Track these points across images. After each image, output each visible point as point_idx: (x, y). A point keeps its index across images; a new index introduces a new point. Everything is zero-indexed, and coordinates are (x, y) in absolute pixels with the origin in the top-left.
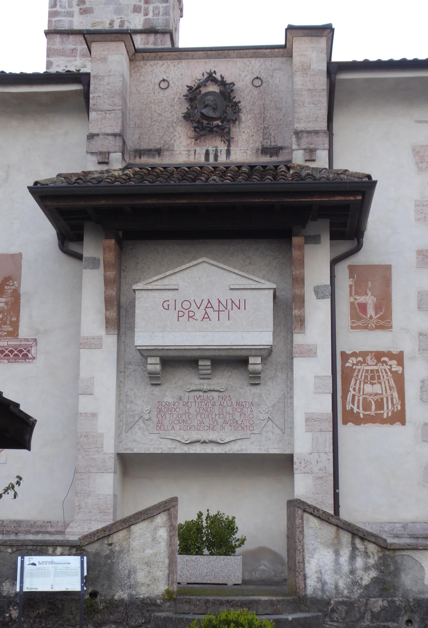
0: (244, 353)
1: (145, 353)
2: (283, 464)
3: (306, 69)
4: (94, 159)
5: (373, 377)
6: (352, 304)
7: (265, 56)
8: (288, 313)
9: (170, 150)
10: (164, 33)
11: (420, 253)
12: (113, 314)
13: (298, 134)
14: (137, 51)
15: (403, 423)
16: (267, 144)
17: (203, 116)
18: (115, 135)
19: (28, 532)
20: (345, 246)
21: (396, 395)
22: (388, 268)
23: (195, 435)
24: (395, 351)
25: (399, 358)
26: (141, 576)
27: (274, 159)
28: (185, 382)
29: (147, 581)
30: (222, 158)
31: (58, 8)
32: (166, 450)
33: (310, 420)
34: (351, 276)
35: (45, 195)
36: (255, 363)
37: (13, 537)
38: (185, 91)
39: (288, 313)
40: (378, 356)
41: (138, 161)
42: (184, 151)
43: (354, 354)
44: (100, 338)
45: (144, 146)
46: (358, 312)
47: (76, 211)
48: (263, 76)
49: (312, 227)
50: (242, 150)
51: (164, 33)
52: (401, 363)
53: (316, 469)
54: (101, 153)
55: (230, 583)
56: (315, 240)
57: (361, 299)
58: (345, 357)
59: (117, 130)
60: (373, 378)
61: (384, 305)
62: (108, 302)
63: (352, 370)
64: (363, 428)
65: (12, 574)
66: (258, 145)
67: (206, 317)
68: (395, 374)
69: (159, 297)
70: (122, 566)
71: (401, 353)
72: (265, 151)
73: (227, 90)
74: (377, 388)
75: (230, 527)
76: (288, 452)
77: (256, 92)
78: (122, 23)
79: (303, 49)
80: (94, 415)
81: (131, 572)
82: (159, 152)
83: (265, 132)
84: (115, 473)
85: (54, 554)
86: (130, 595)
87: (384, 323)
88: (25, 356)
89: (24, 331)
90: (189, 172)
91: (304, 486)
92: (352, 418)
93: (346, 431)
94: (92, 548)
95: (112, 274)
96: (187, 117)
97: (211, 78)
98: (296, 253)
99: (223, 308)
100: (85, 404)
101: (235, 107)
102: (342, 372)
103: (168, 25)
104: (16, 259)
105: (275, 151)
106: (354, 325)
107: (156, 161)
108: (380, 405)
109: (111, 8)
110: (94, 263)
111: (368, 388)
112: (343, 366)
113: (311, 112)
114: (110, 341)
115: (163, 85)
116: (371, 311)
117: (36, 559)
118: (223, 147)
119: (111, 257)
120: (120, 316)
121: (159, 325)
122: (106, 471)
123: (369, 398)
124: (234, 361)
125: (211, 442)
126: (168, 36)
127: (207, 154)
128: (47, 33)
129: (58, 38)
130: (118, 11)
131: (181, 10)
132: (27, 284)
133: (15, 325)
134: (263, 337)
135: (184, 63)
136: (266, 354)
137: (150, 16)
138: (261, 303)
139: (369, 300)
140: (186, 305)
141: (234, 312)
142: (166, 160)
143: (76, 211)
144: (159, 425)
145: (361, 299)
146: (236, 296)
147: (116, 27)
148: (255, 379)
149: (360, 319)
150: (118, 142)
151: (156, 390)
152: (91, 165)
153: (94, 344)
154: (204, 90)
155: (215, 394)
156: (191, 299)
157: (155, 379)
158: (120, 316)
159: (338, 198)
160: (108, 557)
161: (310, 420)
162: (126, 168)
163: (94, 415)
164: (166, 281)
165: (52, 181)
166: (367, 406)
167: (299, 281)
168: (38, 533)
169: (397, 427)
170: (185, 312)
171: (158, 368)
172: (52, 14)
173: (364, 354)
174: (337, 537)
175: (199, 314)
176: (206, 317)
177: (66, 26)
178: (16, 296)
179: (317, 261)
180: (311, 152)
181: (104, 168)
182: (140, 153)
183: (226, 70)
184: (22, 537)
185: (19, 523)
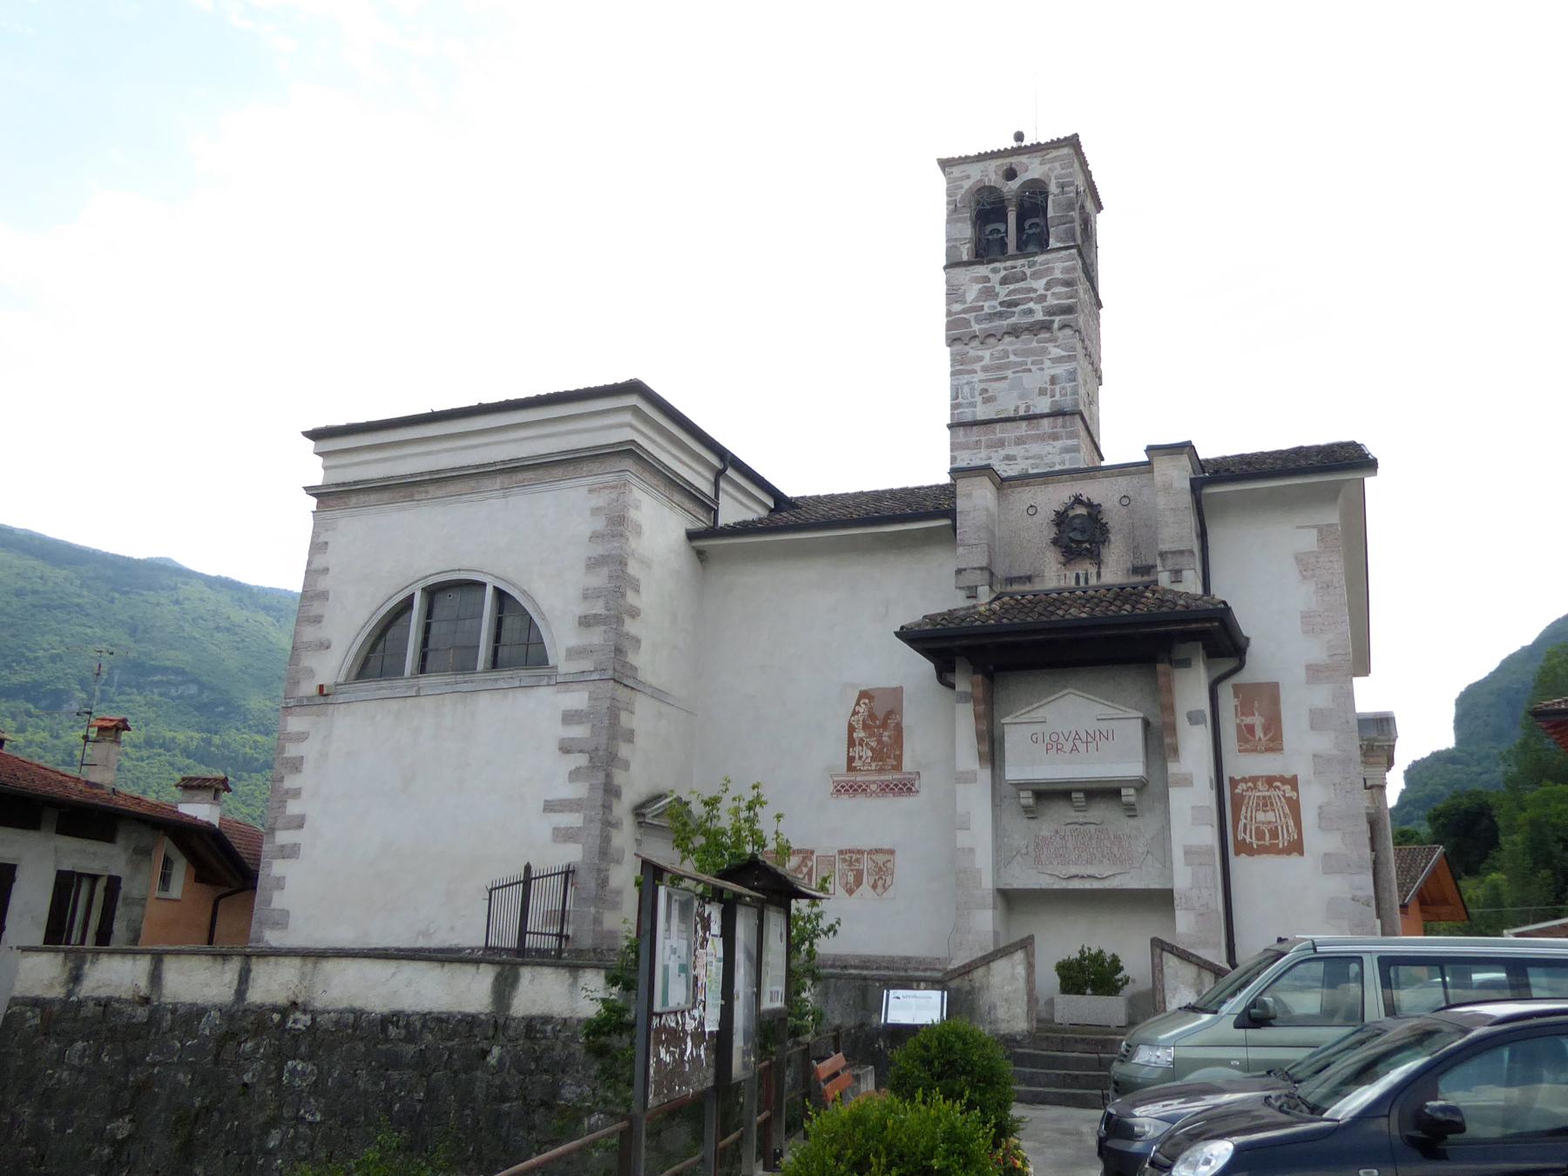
0: (1115, 785)
1: (1020, 786)
2: (1162, 900)
3: (1167, 488)
4: (963, 594)
5: (1265, 804)
6: (1239, 726)
7: (1130, 474)
8: (1159, 740)
9: (1041, 576)
10: (1072, 414)
11: (1309, 667)
12: (986, 748)
13: (1162, 555)
14: (1003, 480)
15: (1302, 854)
16: (1138, 563)
17: (1072, 540)
18: (982, 569)
19: (917, 969)
20: (1227, 664)
21: (1291, 823)
22: (1276, 685)
23: (1073, 870)
24: (1288, 775)
25: (1293, 782)
26: (1001, 1013)
27: (1146, 578)
28: (1059, 816)
29: (1006, 1017)
30: (1093, 581)
31: (960, 400)
32: (1044, 886)
33: (1189, 852)
34: (1236, 696)
35: (912, 637)
36: (1128, 794)
37: (902, 973)
38: (1053, 516)
39: (1159, 740)
40: (1270, 781)
41: (1009, 589)
42: (1054, 575)
43: (1244, 780)
44: (974, 773)
45: (1015, 574)
46: (1246, 733)
47: (944, 645)
48: (1131, 494)
49: (1181, 651)
50: (1113, 571)
51: (1072, 414)
52: (1295, 788)
53: (1197, 906)
54: (969, 588)
55: (1113, 1025)
56: (1186, 663)
57: (1248, 720)
58: (1234, 783)
59: (984, 564)
60: (1265, 805)
61: (1274, 725)
62: (980, 736)
63: (1242, 797)
64: (1257, 859)
65: (878, 1007)
66: (1129, 565)
67: (1075, 749)
68: (1289, 800)
69: (1027, 731)
70: (984, 1001)
71: (1295, 778)
72: (1136, 570)
73: (1094, 510)
74: (1270, 816)
75: (1116, 965)
76: (1168, 886)
77: (1124, 510)
78: (1028, 407)
79: (1163, 466)
80: (972, 850)
81: (992, 1008)
82: (1029, 579)
83: (1136, 551)
84: (995, 908)
85: (918, 988)
86: (991, 1031)
87: (1274, 743)
88: (910, 790)
89: (907, 765)
90: (1059, 598)
91: (1185, 926)
92: (1244, 848)
93: (1238, 863)
94: (954, 984)
95: (981, 708)
96: (1055, 542)
97: (1078, 500)
98: (1162, 680)
99: (1092, 738)
100: (963, 840)
101: (1104, 529)
102: (1227, 797)
103: (1077, 404)
104: (897, 692)
105: (1147, 570)
106: (887, 857)
107: (1027, 587)
108: (1274, 834)
109: (1015, 393)
110: (964, 698)
111: (1261, 816)
112: (1233, 794)
113: (1177, 530)
114: (985, 775)
115: (1031, 511)
116: (1259, 733)
117: (900, 993)
118: (1093, 570)
119: (979, 692)
120: (992, 750)
121: (1028, 762)
122: (984, 907)
123: (1263, 827)
124: (1105, 793)
125: (1090, 876)
126: (1078, 418)
127: (1078, 576)
128: (950, 427)
129: (961, 431)
130: (1022, 396)
131: (1100, 378)
132: (909, 719)
133: (899, 759)
134: (1131, 767)
135: (1051, 487)
136: (1141, 786)
137: (1057, 397)
138: (1132, 732)
139: (1257, 721)
140: (1054, 737)
141: (1103, 744)
142: (1037, 586)
143: (944, 645)
144: (1037, 860)
145: (1248, 720)
146: (1104, 726)
147: (1022, 413)
148: (1131, 810)
149: (1247, 741)
150: (986, 575)
151: (1033, 823)
152: (959, 601)
153: (967, 778)
154: (1071, 513)
155: (1092, 827)
156: (1059, 731)
157: (1030, 813)
158: (992, 750)
159: (1194, 626)
160: (969, 993)
161: (1189, 852)
162: (997, 598)
163: (972, 850)
164: (1033, 714)
165: (918, 625)
166: (1260, 835)
167: (1169, 708)
168: (925, 970)
169: (1294, 858)
170: (1054, 746)
171: (1031, 801)
172: (954, 407)
173: (1254, 779)
174: (1199, 975)
175: (1068, 746)
176: (1075, 749)
177: (969, 418)
178: (899, 729)
179: (1191, 687)
180: (1177, 574)
181: (973, 602)
182: (1011, 581)
183: (1093, 491)
184: (910, 973)
185: (908, 959)
